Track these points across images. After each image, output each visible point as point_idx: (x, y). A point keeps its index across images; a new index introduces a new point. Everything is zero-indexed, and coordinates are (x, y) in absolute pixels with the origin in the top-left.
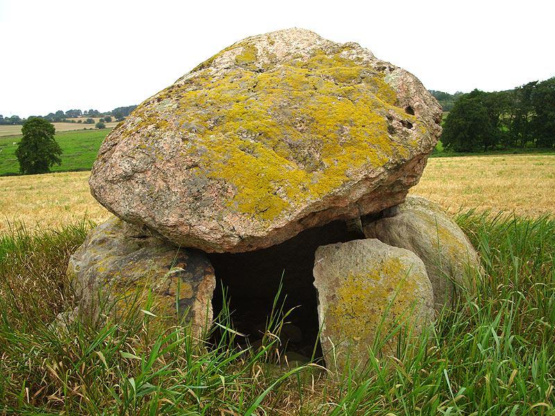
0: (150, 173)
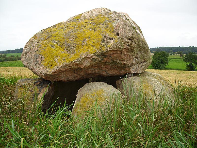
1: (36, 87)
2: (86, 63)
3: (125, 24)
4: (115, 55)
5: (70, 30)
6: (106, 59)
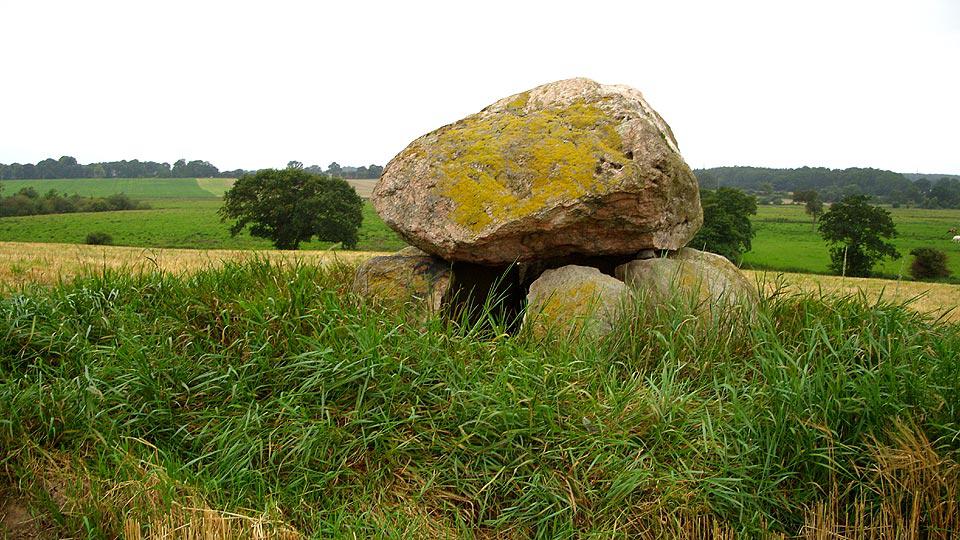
1: (420, 278)
2: (560, 219)
3: (647, 131)
4: (624, 204)
5: (513, 140)
6: (603, 212)
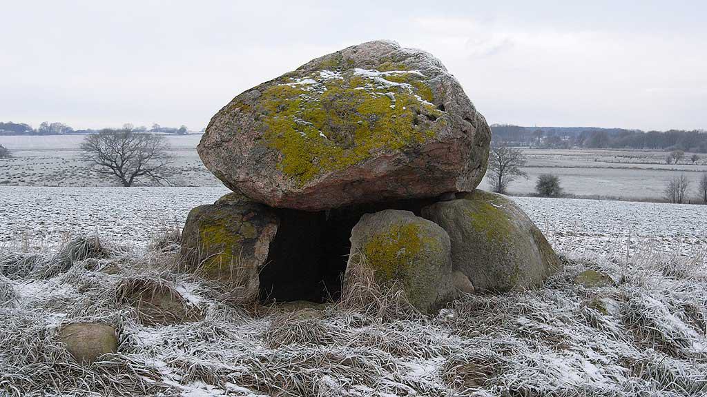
0: (232, 142)
1: (248, 224)
2: (382, 168)
